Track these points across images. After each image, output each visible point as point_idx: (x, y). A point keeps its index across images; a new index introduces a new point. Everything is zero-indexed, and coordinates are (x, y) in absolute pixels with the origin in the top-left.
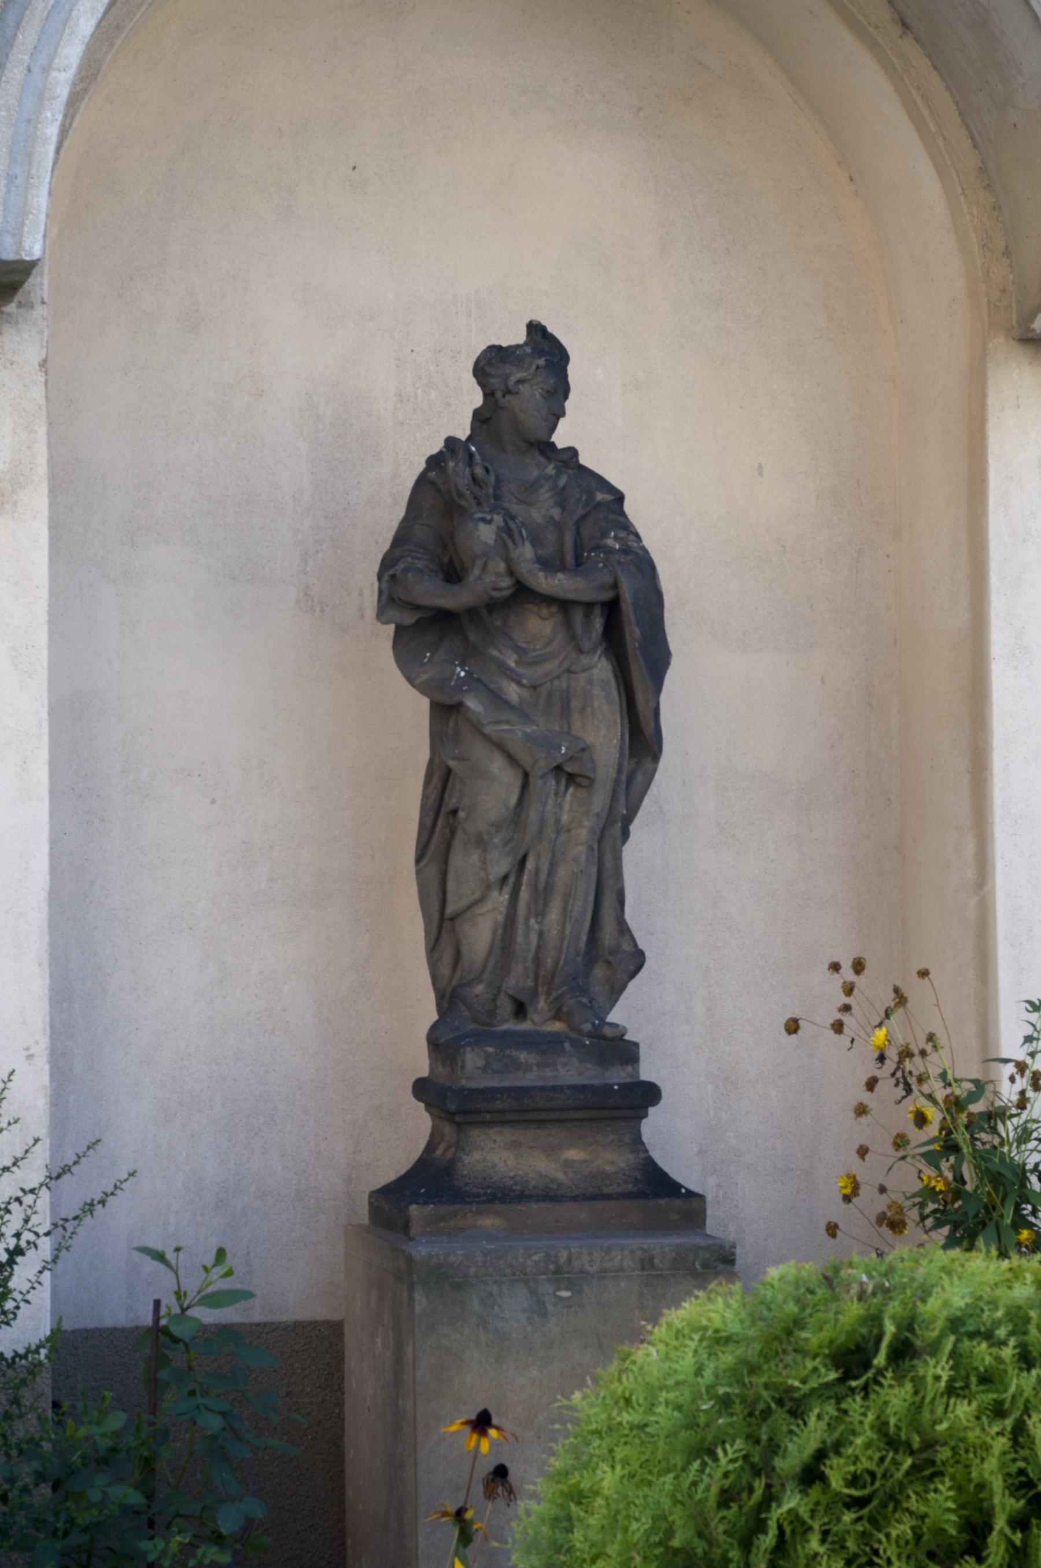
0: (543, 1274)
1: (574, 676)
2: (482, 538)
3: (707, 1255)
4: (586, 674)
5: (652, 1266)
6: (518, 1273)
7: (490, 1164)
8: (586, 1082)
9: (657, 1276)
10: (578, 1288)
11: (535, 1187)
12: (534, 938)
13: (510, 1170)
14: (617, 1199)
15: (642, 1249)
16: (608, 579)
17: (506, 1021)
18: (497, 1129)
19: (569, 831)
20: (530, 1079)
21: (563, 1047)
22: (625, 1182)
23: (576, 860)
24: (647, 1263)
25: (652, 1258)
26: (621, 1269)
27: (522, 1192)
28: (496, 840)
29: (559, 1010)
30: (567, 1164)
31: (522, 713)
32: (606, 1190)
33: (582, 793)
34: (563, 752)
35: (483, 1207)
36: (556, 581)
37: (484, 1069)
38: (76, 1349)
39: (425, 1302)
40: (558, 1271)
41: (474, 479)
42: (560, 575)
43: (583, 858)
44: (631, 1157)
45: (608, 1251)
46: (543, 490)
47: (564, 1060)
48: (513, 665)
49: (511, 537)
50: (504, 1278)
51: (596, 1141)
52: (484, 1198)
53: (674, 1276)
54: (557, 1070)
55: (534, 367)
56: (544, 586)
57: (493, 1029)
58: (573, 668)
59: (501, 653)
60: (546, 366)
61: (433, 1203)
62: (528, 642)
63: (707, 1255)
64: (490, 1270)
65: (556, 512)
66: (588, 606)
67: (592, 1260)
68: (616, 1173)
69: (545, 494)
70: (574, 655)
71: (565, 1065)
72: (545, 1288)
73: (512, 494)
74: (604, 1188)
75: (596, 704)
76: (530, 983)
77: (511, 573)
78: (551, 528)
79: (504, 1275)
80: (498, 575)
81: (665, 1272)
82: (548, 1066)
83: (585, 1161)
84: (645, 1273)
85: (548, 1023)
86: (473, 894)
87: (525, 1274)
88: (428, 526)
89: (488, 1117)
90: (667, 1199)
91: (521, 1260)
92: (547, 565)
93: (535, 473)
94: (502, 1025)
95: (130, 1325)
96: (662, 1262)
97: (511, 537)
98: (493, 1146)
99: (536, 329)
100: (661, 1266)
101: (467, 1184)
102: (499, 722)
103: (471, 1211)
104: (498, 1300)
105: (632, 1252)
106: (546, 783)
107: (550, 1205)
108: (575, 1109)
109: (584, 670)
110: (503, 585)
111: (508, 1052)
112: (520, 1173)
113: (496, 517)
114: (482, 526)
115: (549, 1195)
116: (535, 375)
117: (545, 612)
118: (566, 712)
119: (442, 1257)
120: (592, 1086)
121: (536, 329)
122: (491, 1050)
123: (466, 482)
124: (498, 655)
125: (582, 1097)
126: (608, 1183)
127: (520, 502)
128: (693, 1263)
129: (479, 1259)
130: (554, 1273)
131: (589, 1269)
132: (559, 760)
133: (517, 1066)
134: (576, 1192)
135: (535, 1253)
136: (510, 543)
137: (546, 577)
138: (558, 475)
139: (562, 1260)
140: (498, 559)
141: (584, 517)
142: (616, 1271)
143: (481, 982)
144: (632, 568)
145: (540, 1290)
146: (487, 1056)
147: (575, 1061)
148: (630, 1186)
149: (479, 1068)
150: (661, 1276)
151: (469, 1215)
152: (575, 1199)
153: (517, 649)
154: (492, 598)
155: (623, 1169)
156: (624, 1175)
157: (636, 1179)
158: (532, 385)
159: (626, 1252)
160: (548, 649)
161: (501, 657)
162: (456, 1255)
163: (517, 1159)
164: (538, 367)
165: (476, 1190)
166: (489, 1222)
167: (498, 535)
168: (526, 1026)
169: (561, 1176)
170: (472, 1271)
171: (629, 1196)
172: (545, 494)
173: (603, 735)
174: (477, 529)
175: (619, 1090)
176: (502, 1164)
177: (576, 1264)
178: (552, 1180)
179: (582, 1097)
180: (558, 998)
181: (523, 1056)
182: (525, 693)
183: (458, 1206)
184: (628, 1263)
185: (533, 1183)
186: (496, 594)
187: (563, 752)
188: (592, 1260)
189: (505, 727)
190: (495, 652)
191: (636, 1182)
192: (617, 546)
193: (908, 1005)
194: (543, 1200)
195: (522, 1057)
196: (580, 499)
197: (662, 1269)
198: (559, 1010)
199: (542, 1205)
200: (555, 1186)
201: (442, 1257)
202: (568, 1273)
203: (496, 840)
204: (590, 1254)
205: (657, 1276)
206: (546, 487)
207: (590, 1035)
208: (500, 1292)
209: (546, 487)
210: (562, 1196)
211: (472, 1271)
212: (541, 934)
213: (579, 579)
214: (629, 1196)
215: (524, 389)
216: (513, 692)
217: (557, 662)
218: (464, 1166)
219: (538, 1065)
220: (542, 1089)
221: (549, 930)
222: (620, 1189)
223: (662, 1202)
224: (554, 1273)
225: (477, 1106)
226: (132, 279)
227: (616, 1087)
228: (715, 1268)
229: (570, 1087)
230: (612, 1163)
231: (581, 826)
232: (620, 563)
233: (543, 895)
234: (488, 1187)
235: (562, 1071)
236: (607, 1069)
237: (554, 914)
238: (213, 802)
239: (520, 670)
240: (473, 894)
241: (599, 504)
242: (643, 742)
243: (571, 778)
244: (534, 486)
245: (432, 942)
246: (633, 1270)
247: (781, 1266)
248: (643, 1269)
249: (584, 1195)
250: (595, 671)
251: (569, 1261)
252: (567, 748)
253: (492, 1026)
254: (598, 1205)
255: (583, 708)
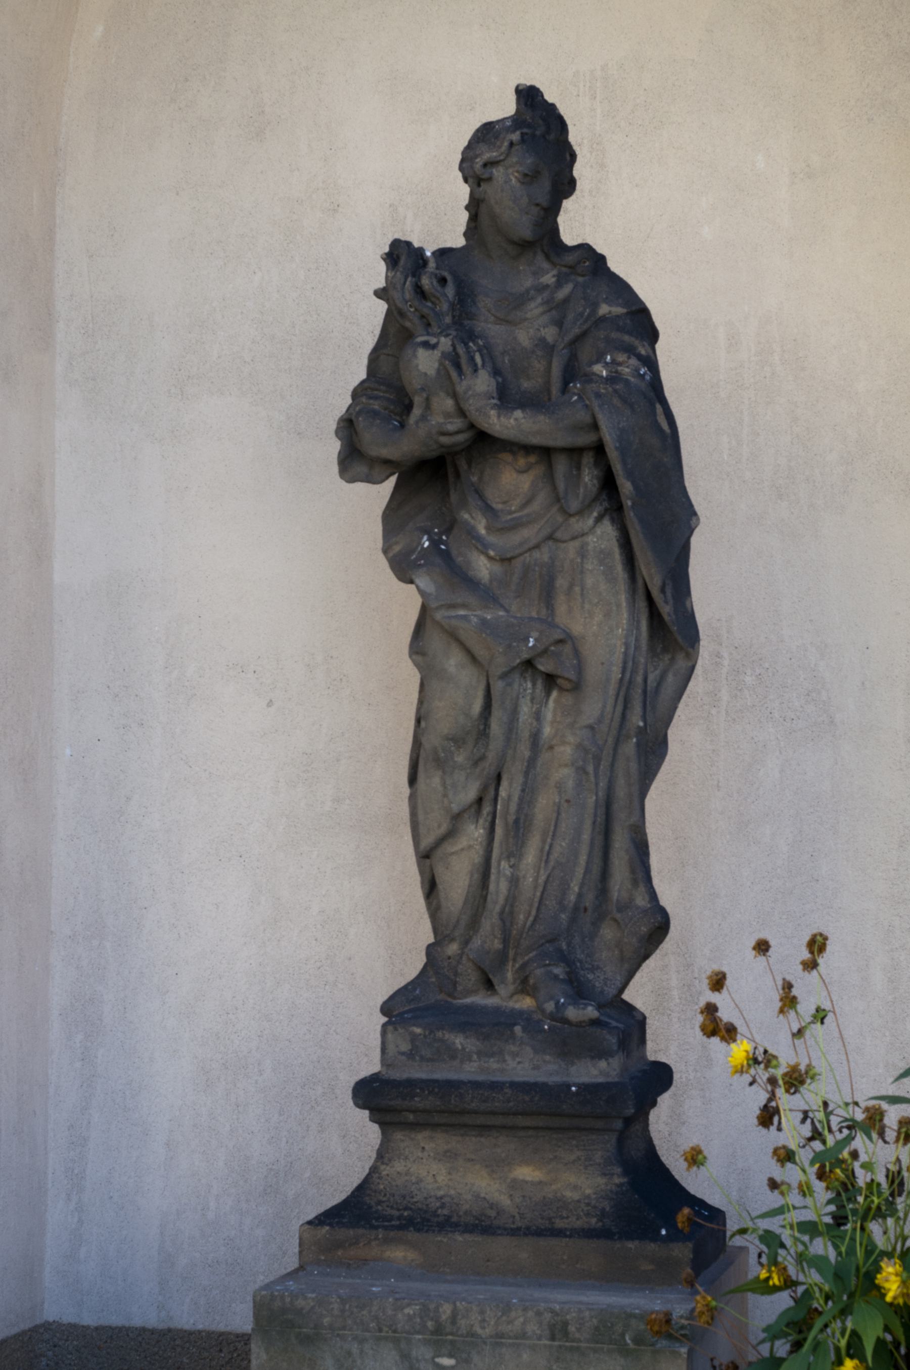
0: (418, 1333)
1: (563, 545)
2: (420, 367)
3: (642, 1327)
4: (576, 543)
5: (566, 1334)
6: (385, 1329)
7: (414, 1179)
8: (542, 1079)
9: (571, 1349)
10: (464, 1356)
11: (466, 1213)
12: (504, 886)
13: (439, 1188)
14: (570, 1236)
15: (552, 1311)
16: (582, 416)
17: (469, 993)
18: (427, 1133)
19: (551, 748)
20: (470, 1071)
21: (512, 1032)
22: (588, 1214)
23: (559, 787)
24: (559, 1330)
25: (565, 1324)
26: (523, 1335)
27: (448, 1218)
28: (460, 758)
29: (525, 981)
30: (515, 1185)
31: (487, 595)
32: (559, 1224)
33: (568, 699)
34: (531, 644)
35: (392, 1234)
36: (512, 421)
37: (410, 1055)
38: (99, 1348)
39: (264, 1356)
40: (438, 1330)
41: (419, 291)
42: (518, 414)
43: (570, 784)
44: (601, 1181)
45: (507, 1308)
46: (533, 305)
47: (514, 1048)
48: (483, 532)
49: (458, 366)
50: (367, 1334)
51: (556, 1157)
52: (397, 1223)
53: (595, 1351)
54: (505, 1061)
55: (506, 144)
56: (498, 427)
57: (455, 1002)
58: (558, 535)
59: (473, 518)
60: (523, 140)
61: (331, 1225)
62: (504, 503)
63: (642, 1327)
64: (349, 1322)
65: (550, 333)
66: (574, 452)
67: (484, 1320)
68: (579, 1201)
69: (534, 309)
70: (560, 519)
71: (514, 1055)
72: (422, 1352)
73: (489, 311)
74: (557, 1221)
75: (589, 581)
76: (497, 945)
77: (462, 412)
78: (539, 353)
79: (368, 1330)
80: (447, 415)
81: (583, 1345)
82: (492, 1055)
83: (540, 1182)
84: (556, 1343)
85: (515, 998)
86: (439, 827)
87: (395, 1331)
88: (392, 355)
89: (411, 1117)
90: (637, 1242)
91: (390, 1312)
92: (506, 398)
93: (529, 282)
94: (466, 997)
95: (162, 1326)
96: (579, 1330)
97: (458, 366)
98: (420, 1154)
99: (529, 96)
100: (577, 1335)
101: (379, 1203)
102: (453, 606)
103: (376, 1239)
104: (359, 1362)
105: (539, 1314)
106: (510, 685)
107: (479, 1239)
108: (524, 1114)
109: (574, 538)
110: (451, 428)
111: (439, 1034)
112: (452, 1192)
113: (443, 339)
114: (422, 353)
115: (483, 1225)
116: (508, 155)
117: (522, 462)
118: (548, 595)
119: (288, 1300)
120: (545, 1084)
121: (529, 96)
122: (418, 1030)
123: (407, 296)
124: (470, 519)
125: (527, 1098)
126: (564, 1214)
127: (500, 321)
128: (623, 1335)
129: (336, 1306)
130: (432, 1333)
131: (479, 1331)
132: (525, 656)
133: (453, 1054)
134: (519, 1224)
135: (409, 1305)
136: (454, 374)
137: (499, 417)
138: (559, 284)
139: (444, 1317)
140: (442, 394)
141: (583, 335)
142: (517, 1338)
143: (453, 940)
144: (616, 401)
145: (414, 1353)
146: (414, 1038)
147: (528, 1050)
148: (594, 1220)
149: (403, 1054)
150: (578, 1348)
151: (373, 1243)
152: (514, 1232)
153: (488, 510)
154: (442, 446)
155: (588, 1197)
156: (588, 1204)
157: (603, 1209)
158: (507, 168)
159: (530, 1314)
160: (526, 511)
161: (472, 521)
162: (305, 1298)
163: (450, 1173)
164: (512, 144)
165: (389, 1211)
166: (398, 1254)
167: (441, 364)
168: (491, 1001)
169: (505, 1201)
170: (326, 1321)
171: (588, 1234)
172: (534, 309)
173: (601, 624)
174: (415, 356)
175: (577, 1093)
176: (430, 1179)
177: (462, 1323)
178: (492, 1206)
179: (527, 1098)
180: (523, 967)
181: (459, 1041)
182: (497, 568)
183: (361, 1231)
184: (532, 1328)
185: (466, 1207)
186: (444, 440)
187: (531, 644)
188: (484, 1320)
189: (462, 612)
190: (466, 516)
191: (603, 1215)
192: (604, 373)
193: (799, 1007)
194: (471, 1232)
195: (457, 1041)
196: (581, 314)
197: (579, 1341)
198: (525, 981)
199: (468, 1237)
200: (493, 1213)
201: (288, 1300)
202: (452, 1334)
203: (460, 758)
204: (482, 1312)
205: (571, 1349)
206: (539, 300)
207: (552, 1017)
208: (362, 1351)
209: (539, 300)
210: (499, 1228)
211: (326, 1321)
212: (514, 881)
213: (541, 418)
214: (588, 1234)
215: (498, 173)
216: (482, 567)
217: (537, 527)
218: (380, 1178)
219: (480, 1054)
220: (476, 1085)
221: (524, 877)
222: (578, 1224)
223: (631, 1245)
224: (432, 1333)
225: (392, 1103)
226: (187, 80)
227: (573, 1089)
228: (653, 1345)
229: (513, 1085)
230: (575, 1188)
231: (564, 743)
232: (598, 395)
233: (520, 828)
234: (406, 1209)
235: (511, 1063)
236: (573, 1064)
237: (530, 857)
238: (270, 703)
239: (492, 539)
240: (439, 827)
241: (603, 319)
242: (669, 630)
243: (550, 680)
244: (521, 300)
245: (427, 886)
246: (539, 1339)
247: (685, 1356)
248: (553, 1338)
249: (528, 1228)
250: (591, 539)
251: (454, 1318)
252: (536, 640)
253: (455, 998)
254: (543, 1242)
255: (571, 586)
